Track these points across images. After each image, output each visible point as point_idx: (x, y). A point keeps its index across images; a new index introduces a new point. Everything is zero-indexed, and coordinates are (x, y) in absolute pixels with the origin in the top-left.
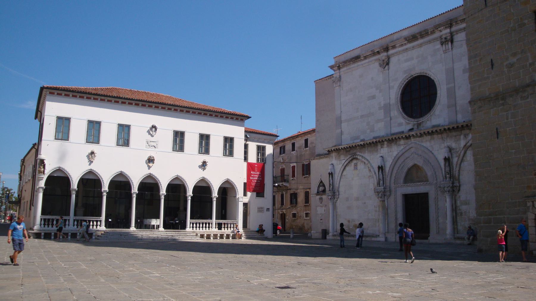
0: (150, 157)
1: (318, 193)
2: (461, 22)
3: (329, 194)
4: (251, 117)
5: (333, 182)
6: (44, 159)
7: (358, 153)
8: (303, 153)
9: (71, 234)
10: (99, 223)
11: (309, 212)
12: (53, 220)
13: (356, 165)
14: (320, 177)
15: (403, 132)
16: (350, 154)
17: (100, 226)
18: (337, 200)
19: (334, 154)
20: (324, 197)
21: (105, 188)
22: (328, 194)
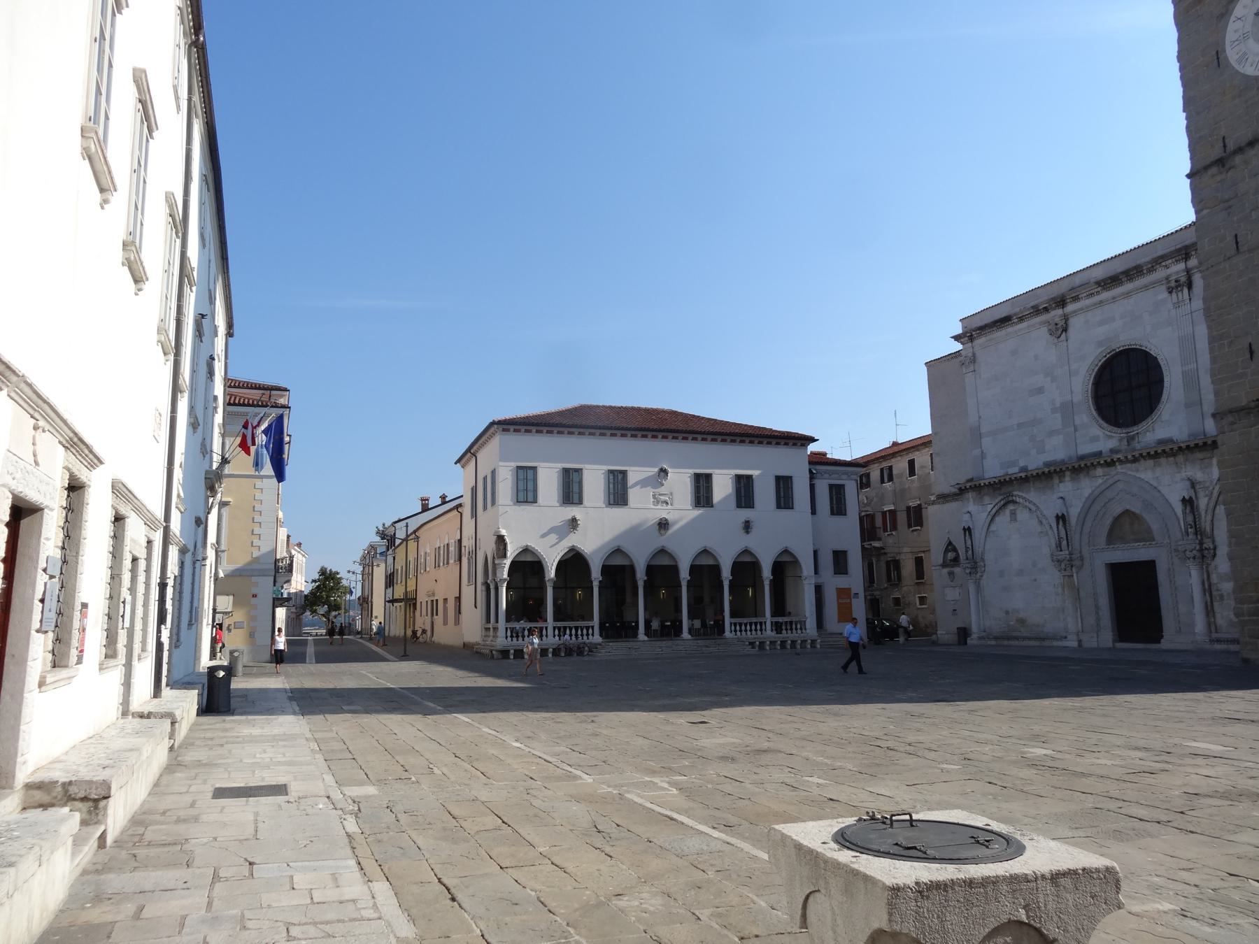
1: (944, 565)
9: (515, 650)
10: (590, 631)
13: (1013, 513)
16: (1000, 495)
17: (593, 635)
19: (970, 495)
20: (957, 570)
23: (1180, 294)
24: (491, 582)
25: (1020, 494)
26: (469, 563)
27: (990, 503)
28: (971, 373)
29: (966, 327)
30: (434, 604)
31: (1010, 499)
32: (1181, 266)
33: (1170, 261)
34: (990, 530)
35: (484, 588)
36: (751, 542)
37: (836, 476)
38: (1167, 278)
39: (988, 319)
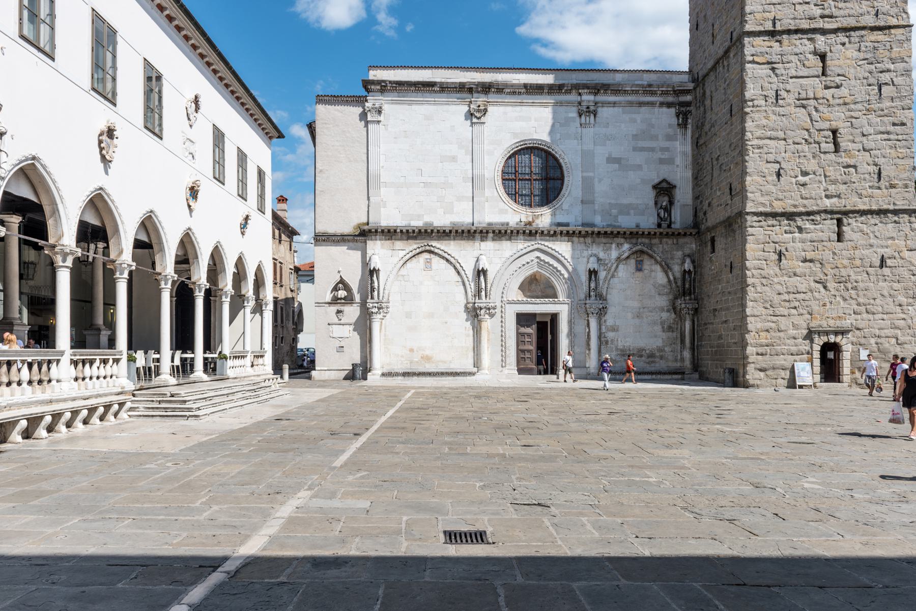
2: (611, 93)
13: (428, 262)
15: (567, 225)
23: (588, 118)
32: (591, 98)
33: (586, 91)
38: (580, 103)
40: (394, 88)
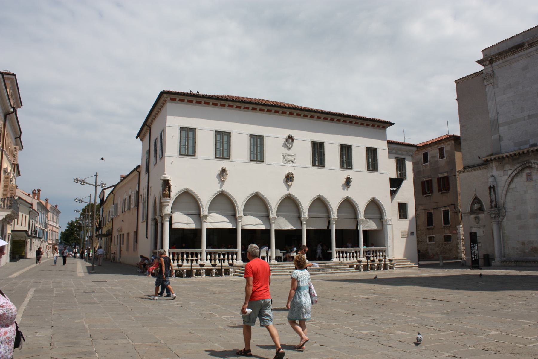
0: (289, 173)
1: (472, 212)
3: (492, 212)
4: (393, 124)
5: (497, 197)
6: (169, 179)
7: (532, 161)
8: (422, 169)
10: (235, 256)
11: (434, 236)
12: (183, 254)
14: (475, 193)
16: (519, 163)
17: (236, 259)
18: (503, 219)
19: (494, 164)
20: (481, 216)
21: (240, 213)
22: (490, 212)
24: (158, 218)
25: (535, 161)
26: (143, 206)
27: (510, 170)
28: (490, 85)
29: (486, 55)
30: (122, 236)
31: (527, 165)
34: (511, 187)
35: (153, 223)
36: (350, 193)
37: (400, 152)
39: (505, 47)
40: (498, 58)
